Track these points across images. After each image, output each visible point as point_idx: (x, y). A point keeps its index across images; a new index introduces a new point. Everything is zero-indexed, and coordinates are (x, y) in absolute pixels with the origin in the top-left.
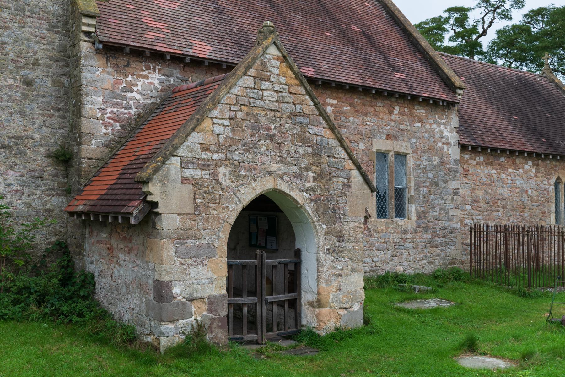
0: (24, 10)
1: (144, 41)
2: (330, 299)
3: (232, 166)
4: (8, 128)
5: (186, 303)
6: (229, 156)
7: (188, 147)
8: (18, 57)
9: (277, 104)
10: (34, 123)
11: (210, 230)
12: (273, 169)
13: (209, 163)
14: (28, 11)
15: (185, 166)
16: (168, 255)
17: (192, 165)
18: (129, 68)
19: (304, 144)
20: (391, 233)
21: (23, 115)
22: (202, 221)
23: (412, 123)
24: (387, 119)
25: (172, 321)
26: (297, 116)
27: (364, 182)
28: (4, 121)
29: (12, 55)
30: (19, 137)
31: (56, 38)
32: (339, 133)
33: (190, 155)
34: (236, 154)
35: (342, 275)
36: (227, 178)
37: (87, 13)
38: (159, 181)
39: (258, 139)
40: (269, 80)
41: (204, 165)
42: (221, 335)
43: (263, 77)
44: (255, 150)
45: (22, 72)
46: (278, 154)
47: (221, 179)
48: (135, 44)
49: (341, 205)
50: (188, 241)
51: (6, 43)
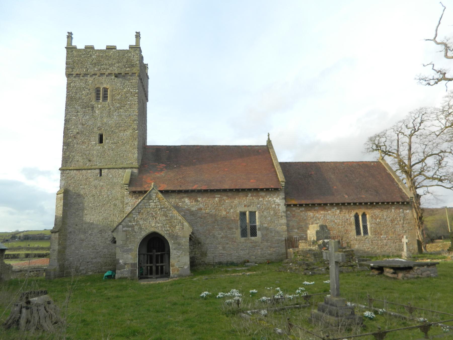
8: (108, 191)
25: (119, 270)
47: (135, 230)
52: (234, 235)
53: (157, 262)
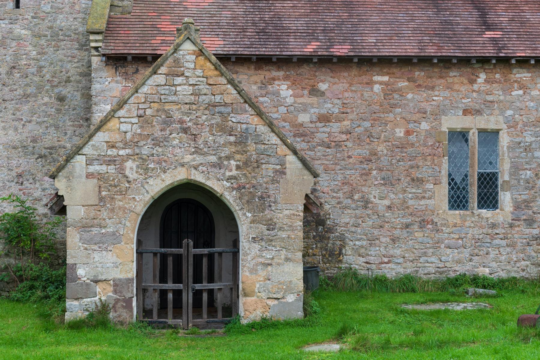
0: (58, 35)
1: (148, 47)
2: (256, 288)
3: (141, 160)
4: (44, 140)
5: (90, 284)
6: (137, 151)
7: (93, 145)
8: (53, 77)
9: (192, 97)
10: (66, 134)
11: (115, 219)
12: (186, 160)
13: (116, 159)
14: (62, 35)
15: (90, 163)
16: (72, 241)
17: (97, 161)
18: (137, 74)
19: (225, 133)
20: (470, 227)
21: (57, 128)
22: (107, 211)
23: (507, 91)
24: (466, 90)
25: (77, 299)
26: (216, 106)
27: (304, 167)
28: (41, 134)
29: (48, 77)
30: (53, 147)
31: (85, 56)
32: (267, 119)
33: (95, 153)
34: (145, 149)
35: (272, 264)
36: (134, 171)
37: (92, 31)
38: (65, 177)
39: (170, 133)
40: (183, 75)
41: (109, 161)
42: (125, 314)
43: (176, 73)
44: (166, 143)
45: (56, 90)
46: (193, 145)
47: (127, 173)
48: (136, 52)
49: (272, 192)
50: (92, 229)
51: (43, 67)
52: (428, 202)
53: (197, 279)
